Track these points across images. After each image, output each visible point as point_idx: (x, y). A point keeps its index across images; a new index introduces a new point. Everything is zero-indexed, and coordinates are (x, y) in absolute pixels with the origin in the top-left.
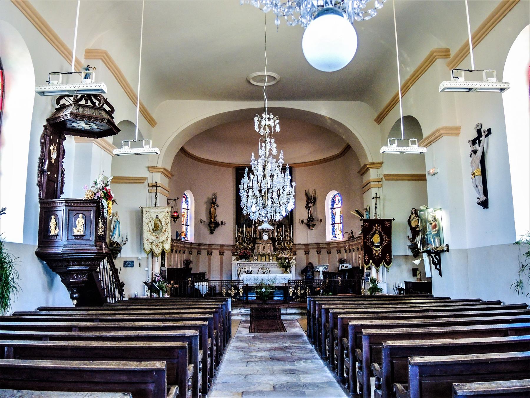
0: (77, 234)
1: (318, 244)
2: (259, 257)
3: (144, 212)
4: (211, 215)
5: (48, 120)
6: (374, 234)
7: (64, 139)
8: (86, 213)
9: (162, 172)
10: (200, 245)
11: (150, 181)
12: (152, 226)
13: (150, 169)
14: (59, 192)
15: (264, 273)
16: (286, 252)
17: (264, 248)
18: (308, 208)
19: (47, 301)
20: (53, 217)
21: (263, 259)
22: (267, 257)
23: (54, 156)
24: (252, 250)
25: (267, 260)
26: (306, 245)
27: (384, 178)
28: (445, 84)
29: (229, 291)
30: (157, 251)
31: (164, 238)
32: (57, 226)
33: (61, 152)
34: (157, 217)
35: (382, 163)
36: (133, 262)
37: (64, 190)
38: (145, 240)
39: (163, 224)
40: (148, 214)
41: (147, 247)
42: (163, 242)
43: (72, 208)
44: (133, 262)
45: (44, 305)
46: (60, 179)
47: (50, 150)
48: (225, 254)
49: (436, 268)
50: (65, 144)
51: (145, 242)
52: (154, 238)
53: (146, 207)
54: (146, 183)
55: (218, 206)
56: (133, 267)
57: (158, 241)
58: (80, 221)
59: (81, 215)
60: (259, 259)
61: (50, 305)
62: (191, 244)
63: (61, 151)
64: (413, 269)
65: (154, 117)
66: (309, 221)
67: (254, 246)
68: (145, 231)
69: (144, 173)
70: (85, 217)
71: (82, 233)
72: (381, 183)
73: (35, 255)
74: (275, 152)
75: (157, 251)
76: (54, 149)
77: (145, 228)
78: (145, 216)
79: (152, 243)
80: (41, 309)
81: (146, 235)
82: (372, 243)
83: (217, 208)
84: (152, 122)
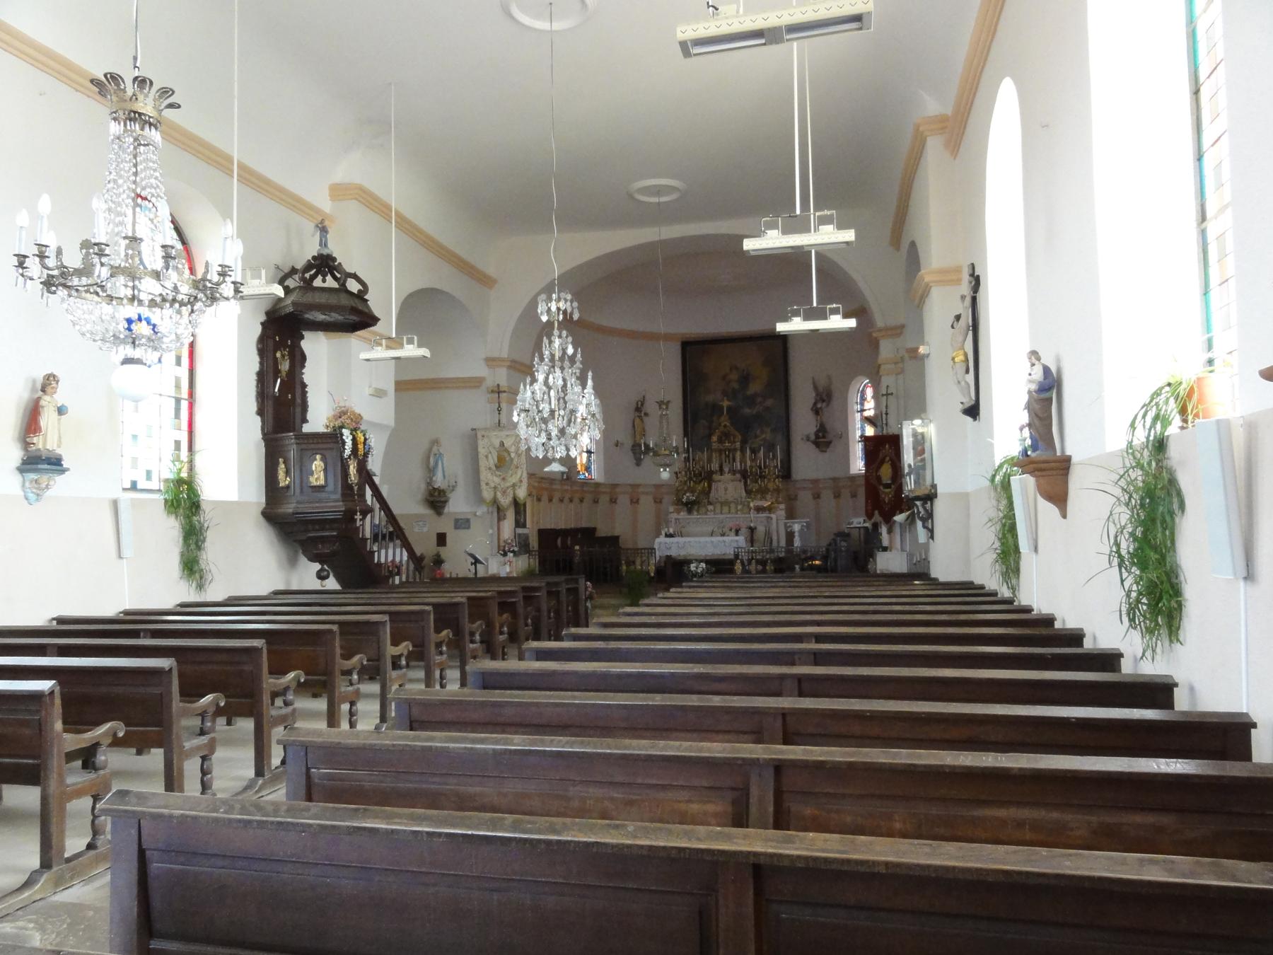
0: (315, 484)
1: (834, 479)
2: (718, 506)
3: (479, 436)
4: (637, 430)
5: (267, 313)
6: (882, 462)
7: (302, 337)
8: (328, 454)
9: (510, 367)
10: (615, 486)
11: (490, 383)
12: (493, 460)
13: (491, 361)
14: (298, 420)
15: (723, 535)
16: (768, 496)
17: (726, 489)
18: (817, 412)
19: (288, 582)
20: (281, 460)
21: (726, 509)
22: (733, 506)
23: (285, 366)
24: (707, 492)
25: (733, 510)
26: (815, 482)
27: (906, 356)
28: (364, 356)
29: (760, 567)
30: (505, 501)
31: (514, 480)
32: (287, 473)
33: (299, 359)
34: (502, 444)
35: (903, 326)
36: (468, 521)
37: (309, 416)
38: (483, 484)
39: (513, 455)
40: (486, 440)
41: (487, 494)
42: (514, 486)
43: (304, 446)
44: (468, 521)
45: (281, 587)
46: (299, 401)
47: (275, 359)
48: (641, 501)
49: (924, 527)
50: (303, 344)
51: (484, 486)
52: (497, 480)
53: (486, 429)
54: (483, 388)
55: (646, 414)
56: (469, 528)
57: (504, 485)
58: (317, 464)
59: (318, 457)
60: (718, 510)
61: (294, 587)
62: (597, 485)
63: (298, 357)
64: (617, 538)
65: (491, 271)
66: (817, 436)
67: (710, 487)
68: (482, 469)
69: (480, 370)
70: (324, 459)
71: (322, 482)
72: (900, 365)
73: (261, 519)
74: (570, 351)
75: (505, 501)
76: (283, 356)
77: (483, 463)
78: (481, 443)
79: (495, 488)
80: (277, 593)
81: (485, 475)
82: (879, 479)
83: (646, 419)
84: (485, 280)
